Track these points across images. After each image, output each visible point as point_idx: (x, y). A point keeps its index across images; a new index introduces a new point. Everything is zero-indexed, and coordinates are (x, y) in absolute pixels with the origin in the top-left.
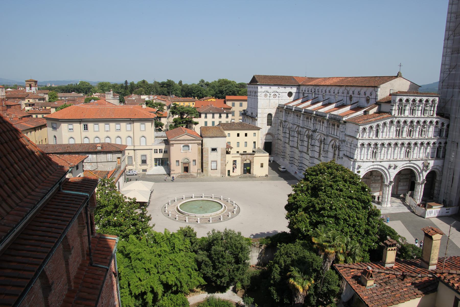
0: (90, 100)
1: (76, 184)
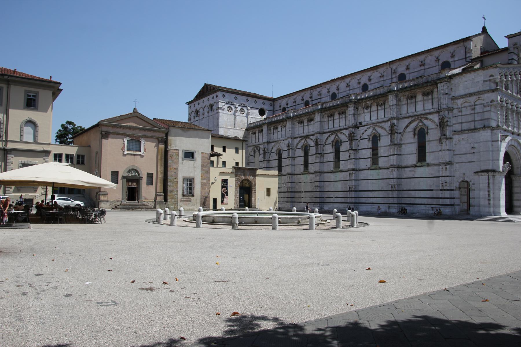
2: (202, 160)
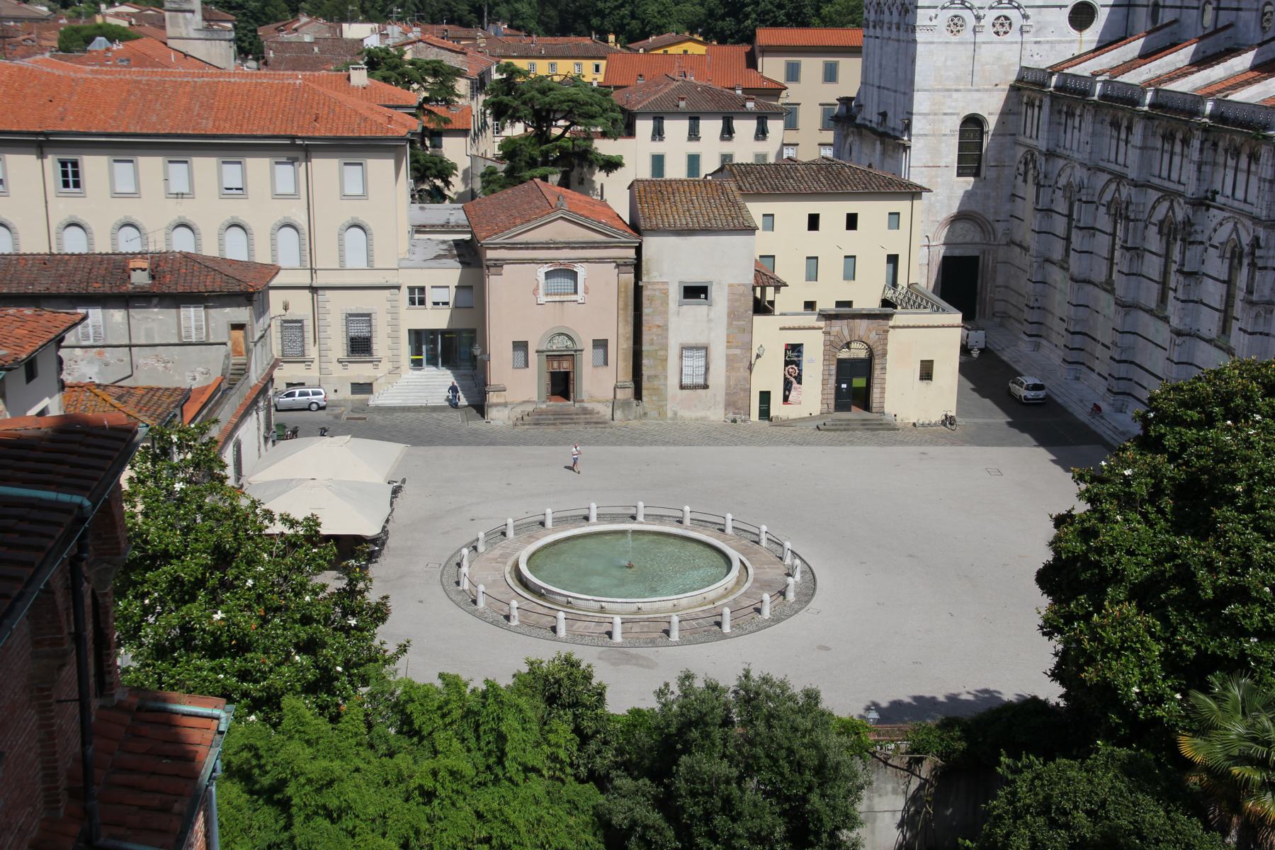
0: (89, 40)
1: (23, 452)
2: (731, 301)
